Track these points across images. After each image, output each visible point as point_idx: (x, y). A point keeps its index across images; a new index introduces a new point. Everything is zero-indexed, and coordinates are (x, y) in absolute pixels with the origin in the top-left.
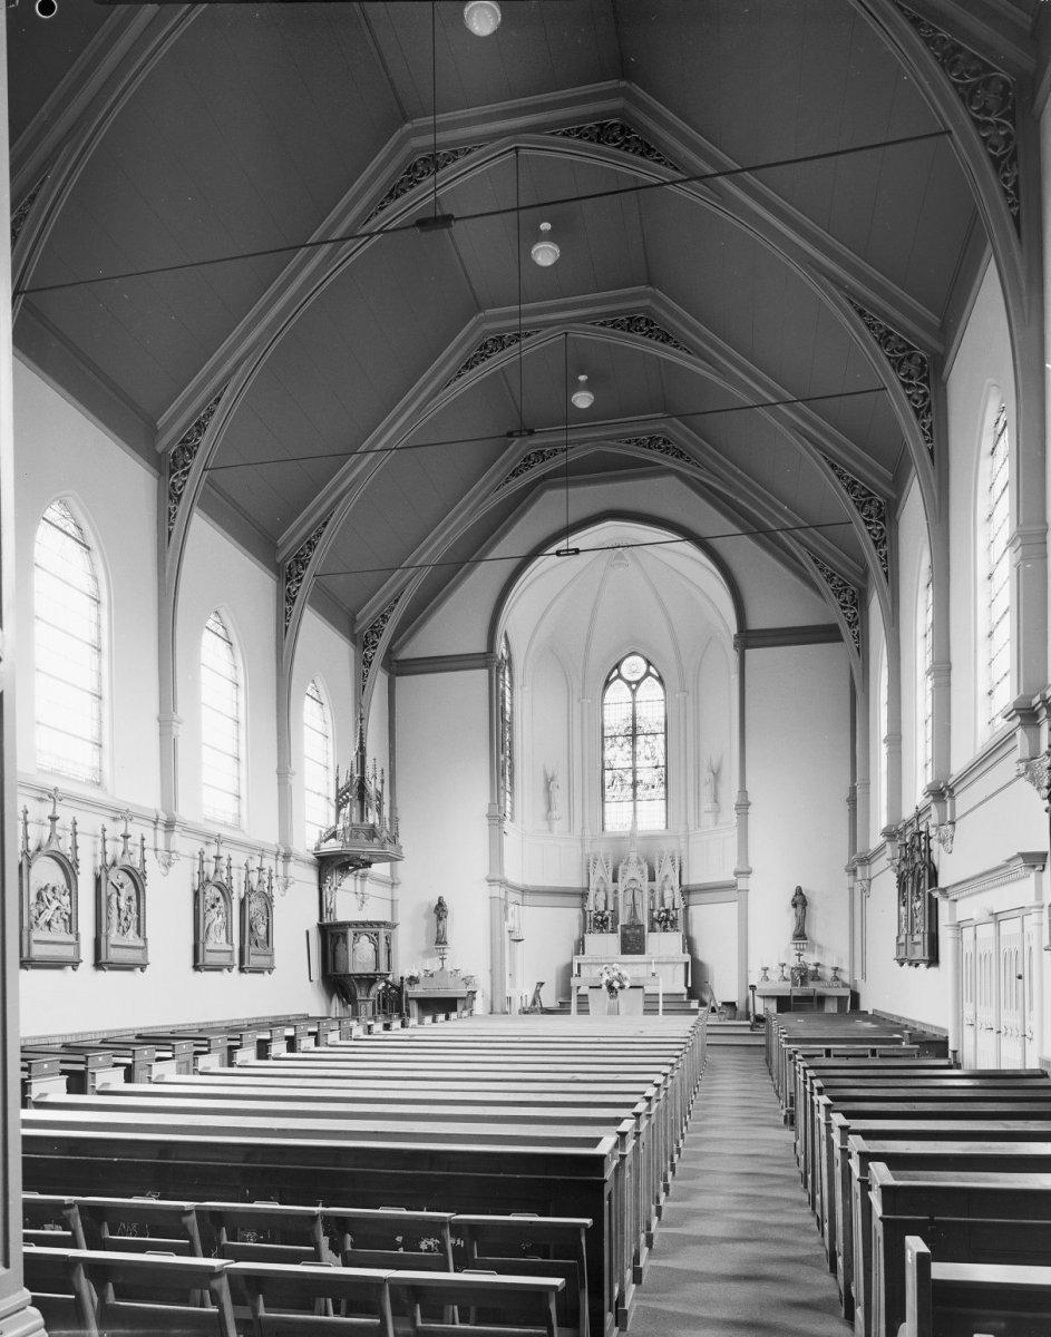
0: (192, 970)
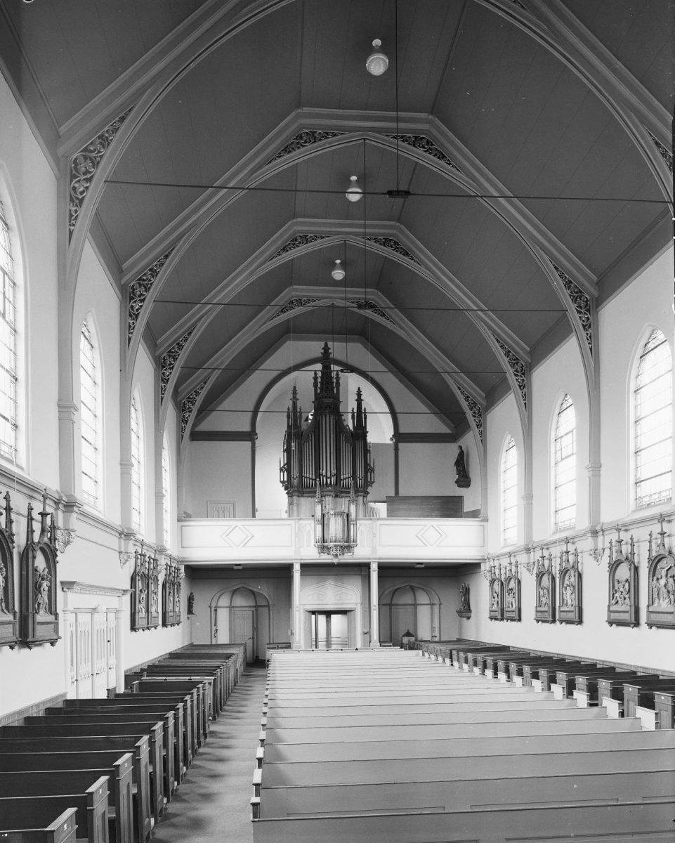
0: (130, 631)
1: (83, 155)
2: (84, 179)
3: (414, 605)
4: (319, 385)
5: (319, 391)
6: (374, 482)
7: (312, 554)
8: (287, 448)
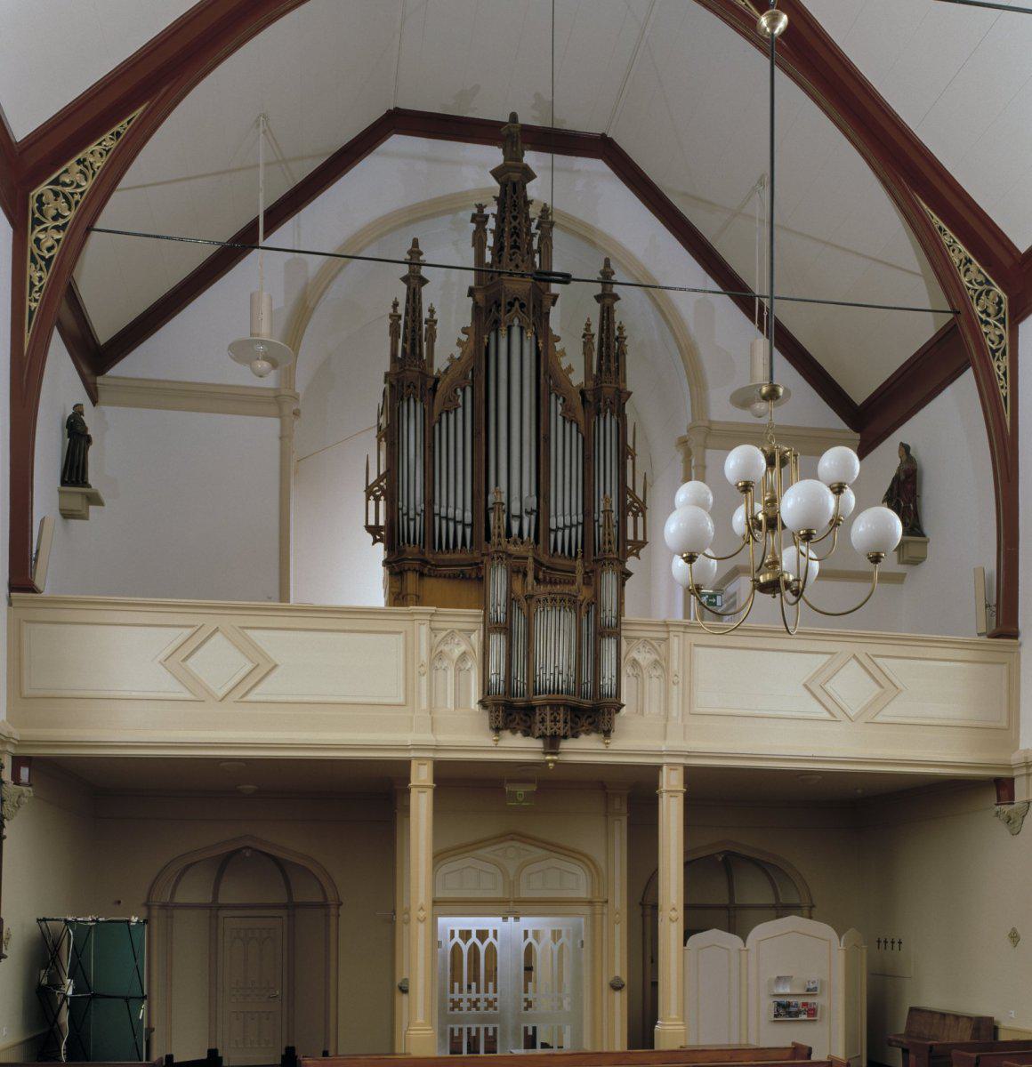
1: (51, 189)
2: (53, 228)
3: (726, 908)
4: (490, 241)
5: (488, 258)
6: (644, 543)
7: (468, 734)
8: (388, 470)
